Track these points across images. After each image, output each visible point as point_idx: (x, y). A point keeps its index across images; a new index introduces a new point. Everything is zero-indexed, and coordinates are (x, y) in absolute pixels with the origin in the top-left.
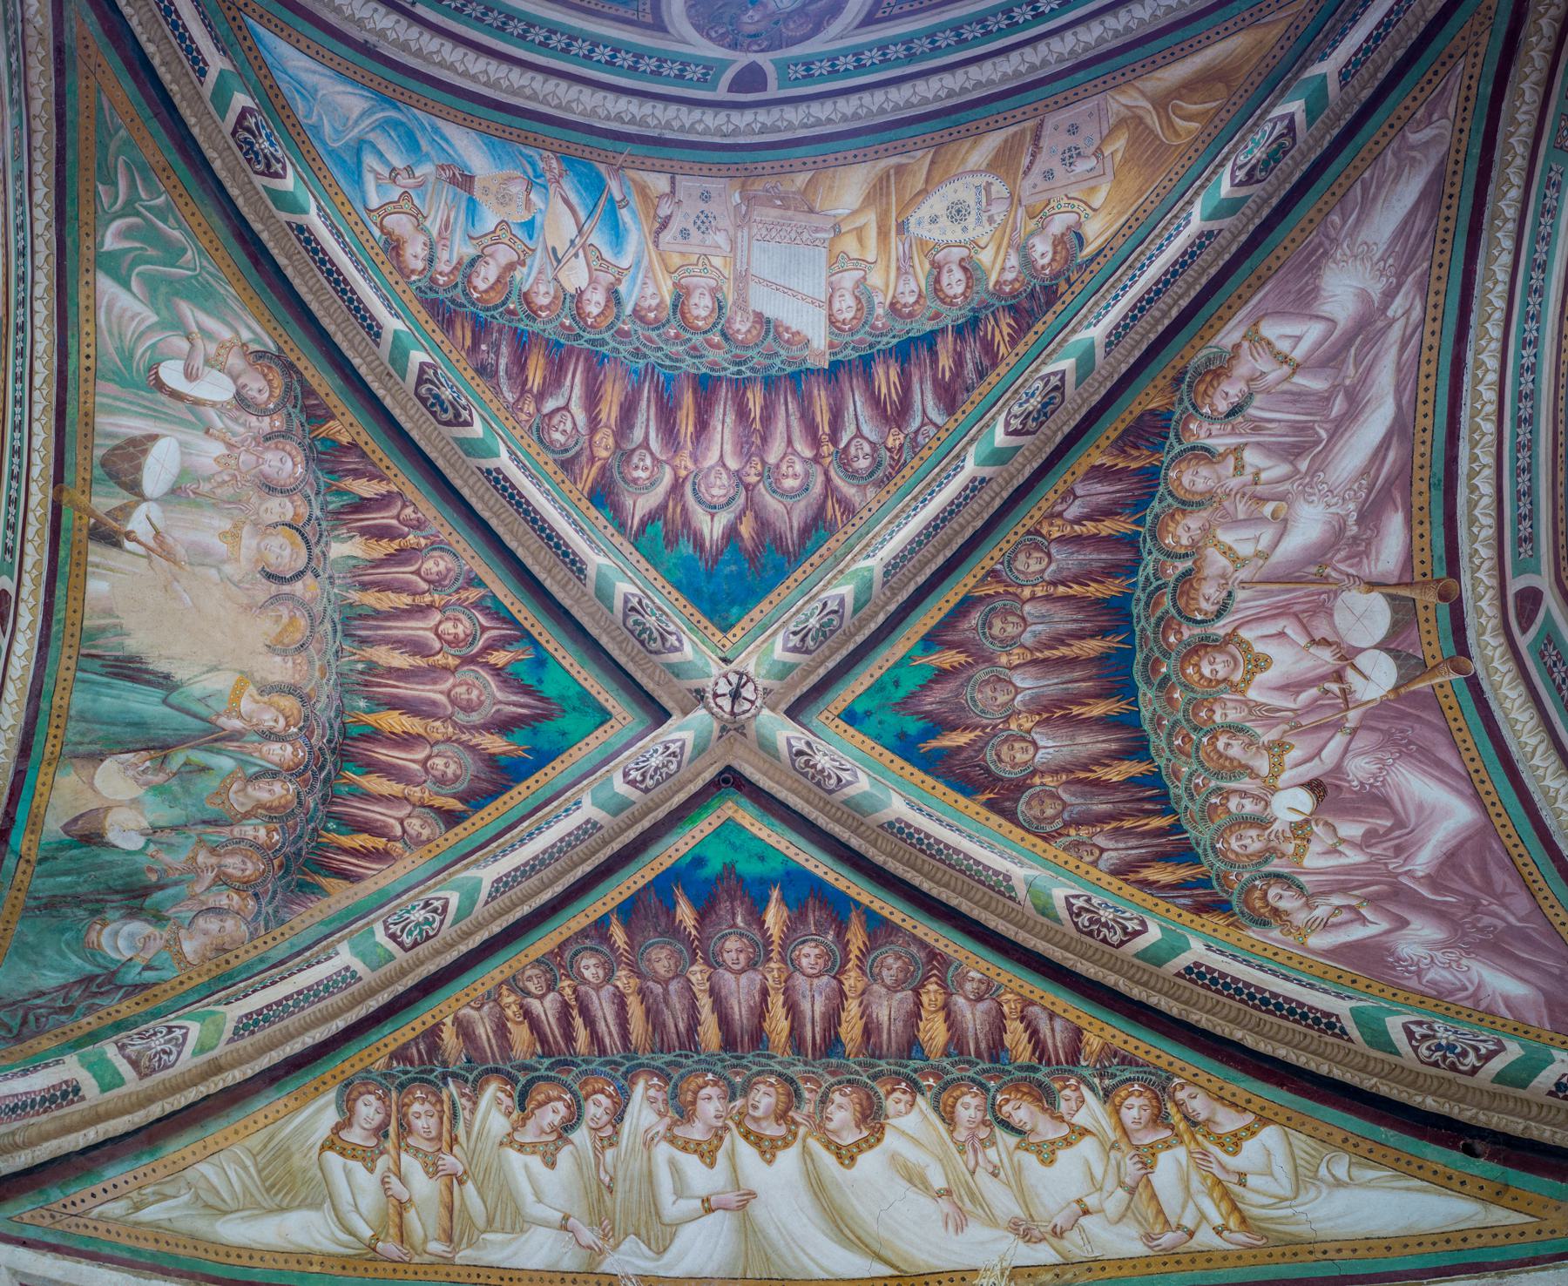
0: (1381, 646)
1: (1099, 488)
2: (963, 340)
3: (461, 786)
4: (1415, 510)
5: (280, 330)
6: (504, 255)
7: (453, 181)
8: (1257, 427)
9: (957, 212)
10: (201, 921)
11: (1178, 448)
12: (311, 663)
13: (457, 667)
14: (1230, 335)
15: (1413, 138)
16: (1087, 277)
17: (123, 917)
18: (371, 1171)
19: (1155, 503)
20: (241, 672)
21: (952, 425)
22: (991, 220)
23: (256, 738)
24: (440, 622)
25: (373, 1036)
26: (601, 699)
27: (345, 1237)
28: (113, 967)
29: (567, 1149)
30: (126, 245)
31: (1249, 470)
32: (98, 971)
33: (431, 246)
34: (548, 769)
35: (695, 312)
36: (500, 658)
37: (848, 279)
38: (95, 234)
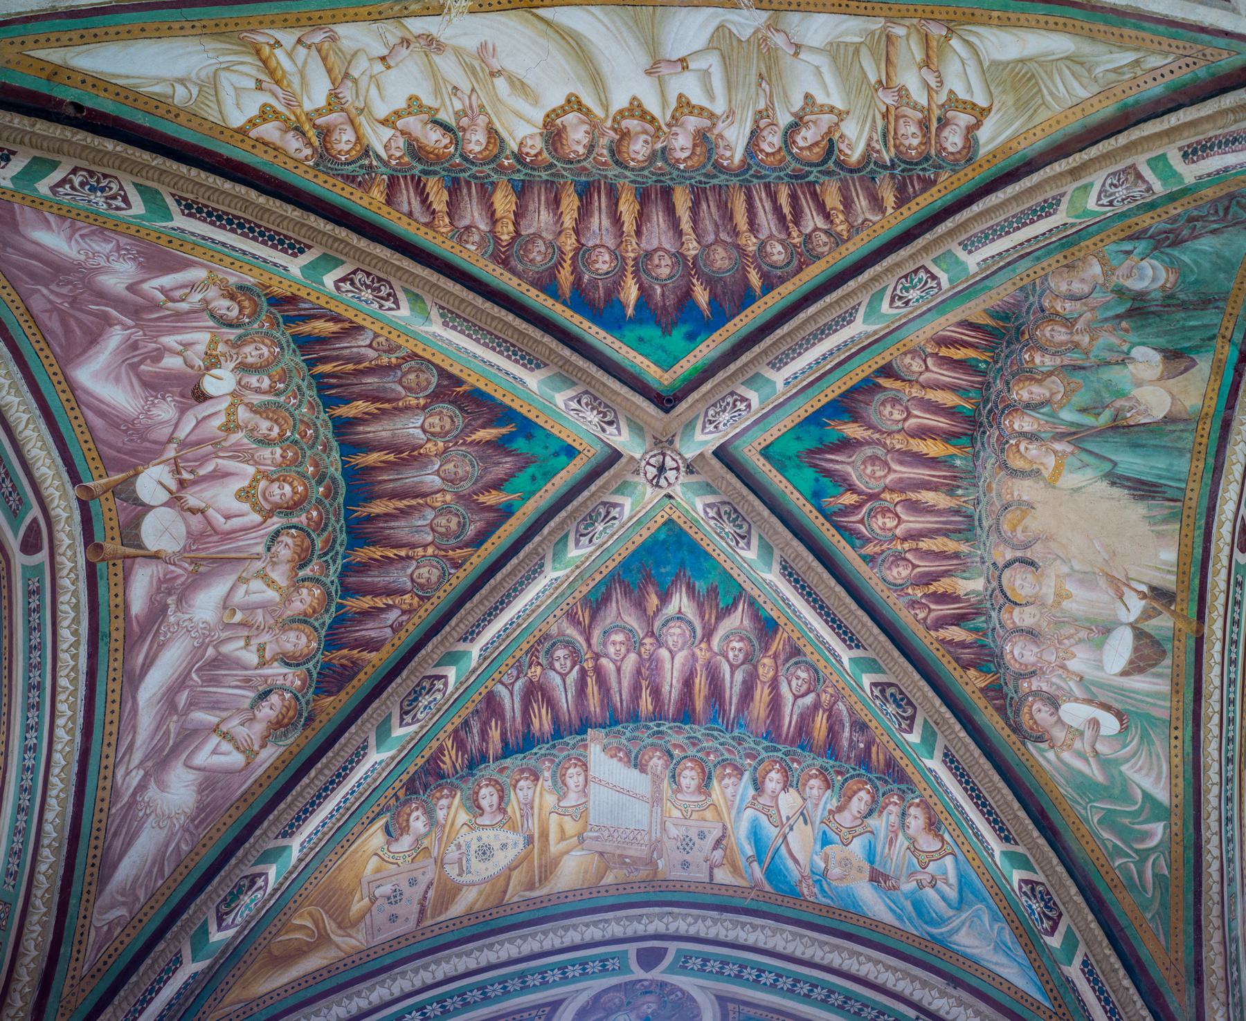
0: (148, 508)
1: (373, 634)
2: (481, 751)
3: (880, 397)
4: (122, 616)
5: (1023, 759)
6: (845, 819)
7: (886, 878)
8: (247, 682)
9: (485, 852)
10: (1087, 289)
11: (310, 665)
12: (999, 495)
13: (883, 491)
15: (123, 911)
16: (383, 801)
17: (1148, 293)
18: (951, 92)
19: (328, 622)
20: (1054, 487)
21: (490, 683)
22: (459, 846)
23: (1043, 435)
24: (896, 527)
25: (949, 198)
26: (768, 467)
28: (1156, 253)
29: (796, 109)
30: (1146, 827)
31: (254, 648)
32: (1168, 250)
33: (904, 826)
34: (811, 410)
35: (693, 773)
36: (849, 499)
37: (572, 799)
38: (1170, 836)
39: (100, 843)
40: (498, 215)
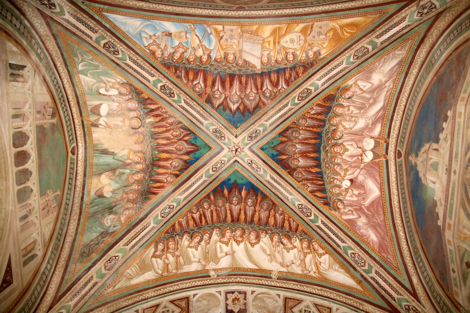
0: (371, 150)
1: (318, 108)
2: (292, 71)
3: (179, 168)
6: (181, 50)
7: (166, 35)
8: (354, 102)
9: (292, 41)
10: (125, 212)
11: (336, 103)
12: (144, 145)
14: (350, 82)
15: (397, 52)
16: (320, 62)
19: (330, 114)
21: (288, 89)
22: (300, 44)
27: (156, 275)
29: (200, 246)
30: (85, 68)
31: (351, 111)
32: (104, 230)
33: (162, 51)
35: (229, 59)
36: (186, 138)
37: (266, 53)
38: (75, 66)
39: (400, 70)
40: (273, 218)
